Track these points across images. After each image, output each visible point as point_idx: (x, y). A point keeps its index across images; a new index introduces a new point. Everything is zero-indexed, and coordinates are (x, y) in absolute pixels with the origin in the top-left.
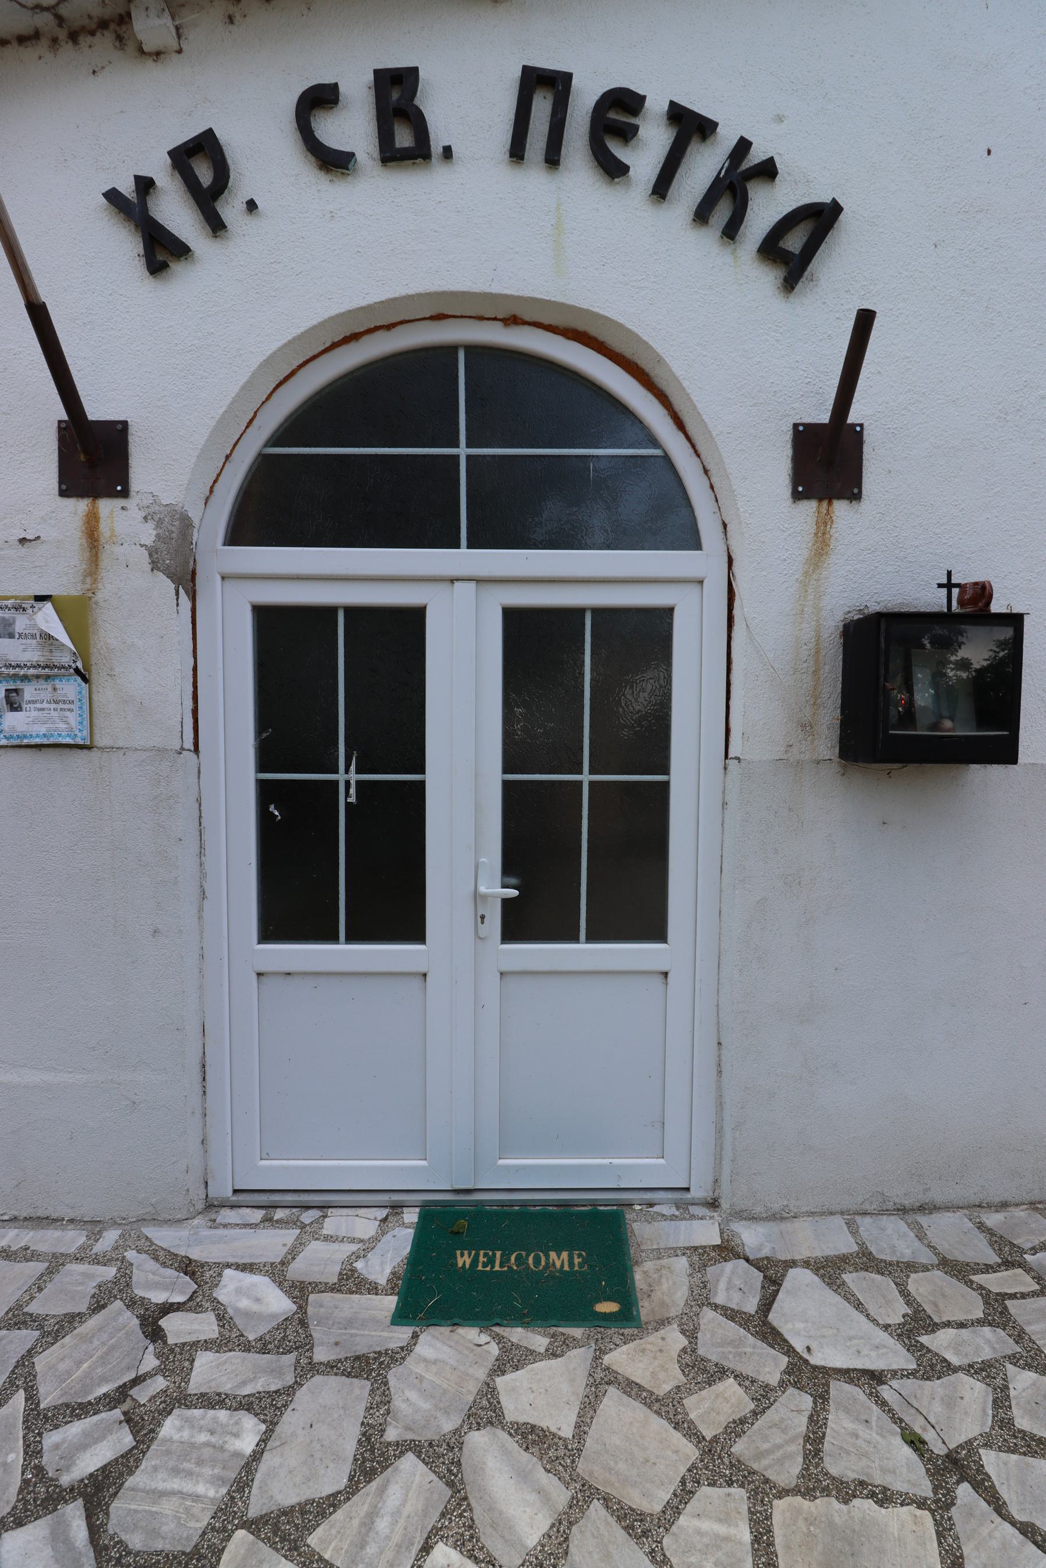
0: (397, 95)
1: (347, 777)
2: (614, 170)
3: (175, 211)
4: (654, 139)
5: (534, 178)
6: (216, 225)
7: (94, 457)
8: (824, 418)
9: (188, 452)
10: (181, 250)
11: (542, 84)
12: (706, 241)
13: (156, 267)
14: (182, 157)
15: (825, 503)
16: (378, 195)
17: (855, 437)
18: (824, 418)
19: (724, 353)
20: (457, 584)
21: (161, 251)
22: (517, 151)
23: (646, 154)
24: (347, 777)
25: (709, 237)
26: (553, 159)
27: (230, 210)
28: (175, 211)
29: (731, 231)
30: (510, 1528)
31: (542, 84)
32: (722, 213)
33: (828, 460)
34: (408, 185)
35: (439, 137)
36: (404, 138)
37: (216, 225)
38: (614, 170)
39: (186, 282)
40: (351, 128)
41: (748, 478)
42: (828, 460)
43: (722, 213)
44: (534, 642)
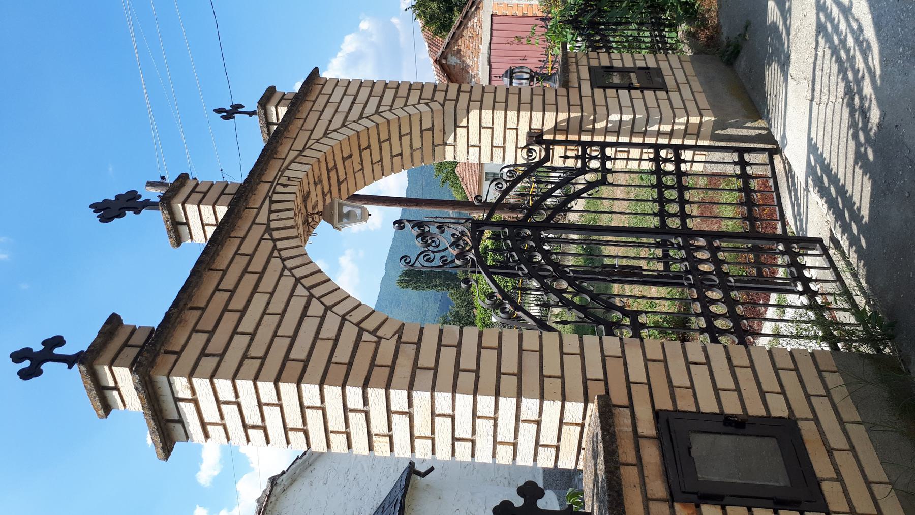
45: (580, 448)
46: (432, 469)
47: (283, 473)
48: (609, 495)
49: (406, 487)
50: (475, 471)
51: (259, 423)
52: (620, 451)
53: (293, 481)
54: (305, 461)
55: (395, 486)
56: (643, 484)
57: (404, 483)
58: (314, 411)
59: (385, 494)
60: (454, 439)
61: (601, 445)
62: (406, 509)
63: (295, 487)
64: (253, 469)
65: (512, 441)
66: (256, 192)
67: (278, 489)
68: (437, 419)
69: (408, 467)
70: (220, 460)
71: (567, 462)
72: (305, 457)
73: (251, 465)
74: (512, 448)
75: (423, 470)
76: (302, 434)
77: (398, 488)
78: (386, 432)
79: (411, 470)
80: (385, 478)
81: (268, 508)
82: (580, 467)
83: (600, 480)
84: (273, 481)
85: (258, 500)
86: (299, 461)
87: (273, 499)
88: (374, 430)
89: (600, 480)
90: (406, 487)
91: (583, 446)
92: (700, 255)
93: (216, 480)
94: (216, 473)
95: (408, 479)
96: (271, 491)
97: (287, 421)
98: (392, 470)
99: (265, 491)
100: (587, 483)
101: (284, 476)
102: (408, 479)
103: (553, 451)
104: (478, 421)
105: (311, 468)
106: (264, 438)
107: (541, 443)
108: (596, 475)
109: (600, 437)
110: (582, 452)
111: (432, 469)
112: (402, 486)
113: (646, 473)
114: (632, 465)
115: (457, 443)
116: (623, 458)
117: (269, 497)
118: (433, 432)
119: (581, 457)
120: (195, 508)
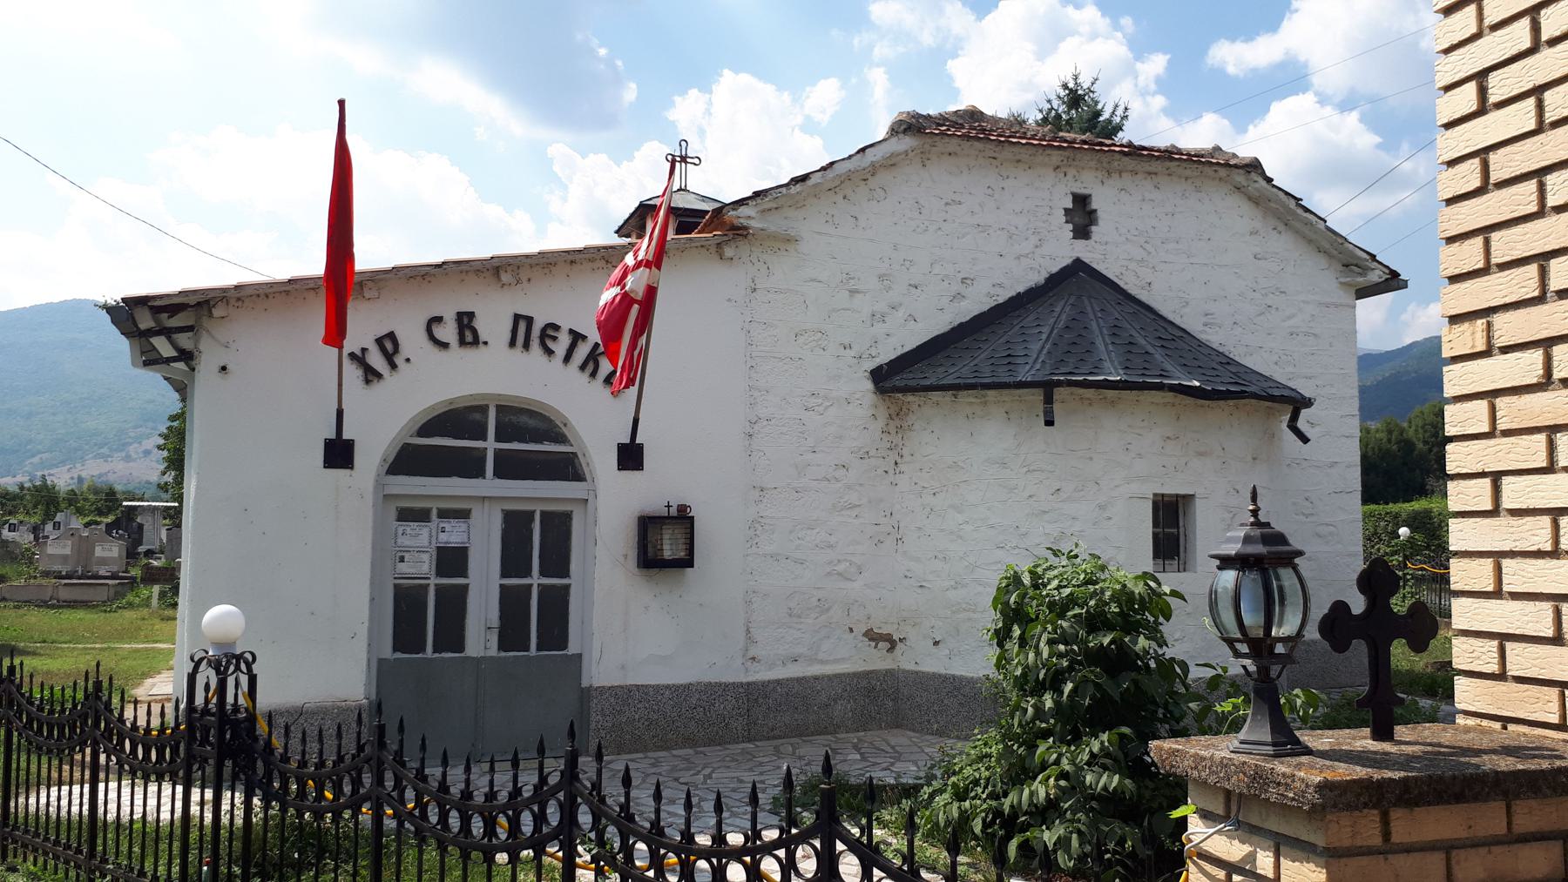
0: (465, 321)
1: (536, 580)
2: (549, 352)
3: (376, 360)
4: (564, 340)
5: (518, 351)
6: (393, 366)
7: (339, 453)
8: (628, 441)
9: (372, 451)
10: (379, 376)
11: (521, 321)
12: (584, 377)
13: (367, 382)
14: (379, 342)
15: (1398, 711)
16: (458, 356)
17: (641, 447)
18: (628, 441)
19: (590, 414)
20: (487, 503)
21: (371, 375)
22: (512, 343)
23: (560, 348)
24: (536, 580)
25: (585, 377)
26: (526, 346)
27: (399, 360)
28: (376, 360)
29: (593, 375)
30: (1048, 388)
31: (521, 321)
32: (591, 366)
33: (630, 456)
34: (470, 354)
35: (483, 337)
36: (469, 338)
37: (393, 366)
38: (549, 352)
39: (378, 387)
40: (448, 332)
41: (601, 460)
42: (630, 456)
43: (591, 366)
44: (515, 525)
45: (1506, 721)
46: (1305, 440)
47: (1269, 180)
48: (1454, 777)
49: (1272, 398)
50: (1302, 518)
51: (1493, 99)
52: (1533, 803)
53: (1255, 200)
54: (1294, 213)
55: (1267, 379)
56: (1475, 844)
57: (1276, 393)
58: (1534, 197)
59: (1249, 362)
60: (1496, 477)
61: (1545, 765)
62: (1231, 402)
63: (1246, 207)
64: (1245, 131)
65: (1506, 588)
66: (1302, 58)
67: (1239, 177)
68: (1542, 437)
69: (1303, 397)
70: (1254, 70)
71: (1466, 694)
72: (1300, 211)
73: (1251, 127)
74: (1490, 588)
75: (1301, 424)
76: (1476, 183)
77: (1265, 385)
78: (1500, 342)
79: (1298, 403)
80: (1275, 358)
81: (1207, 169)
82: (1461, 720)
83: (1474, 760)
84: (1254, 166)
85: (1217, 149)
86: (1292, 204)
87: (1223, 172)
88: (1499, 320)
89: (1474, 760)
90: (1272, 398)
91: (1511, 727)
92: (529, 780)
93: (1219, 73)
94: (1231, 69)
95: (1282, 399)
96: (1236, 166)
97: (1502, 151)
98: (1291, 369)
99: (1234, 156)
100: (1429, 732)
101: (1264, 183)
102: (1282, 399)
103: (1493, 668)
104: (1546, 521)
105: (1281, 227)
106: (1457, 116)
107: (1509, 646)
108: (1478, 752)
109: (1558, 763)
110: (1497, 726)
111: (1305, 440)
112: (1270, 391)
113: (1496, 849)
114: (1509, 824)
115: (1487, 482)
116: (1520, 807)
117: (1227, 165)
118: (1508, 433)
119: (1485, 723)
120: (1165, 53)
